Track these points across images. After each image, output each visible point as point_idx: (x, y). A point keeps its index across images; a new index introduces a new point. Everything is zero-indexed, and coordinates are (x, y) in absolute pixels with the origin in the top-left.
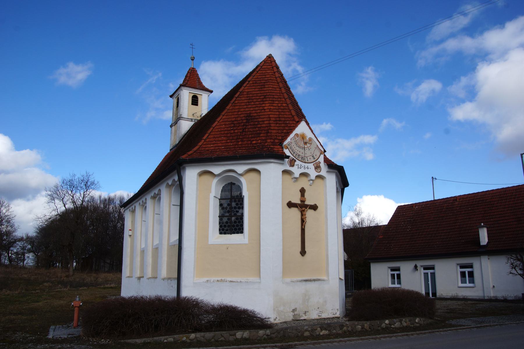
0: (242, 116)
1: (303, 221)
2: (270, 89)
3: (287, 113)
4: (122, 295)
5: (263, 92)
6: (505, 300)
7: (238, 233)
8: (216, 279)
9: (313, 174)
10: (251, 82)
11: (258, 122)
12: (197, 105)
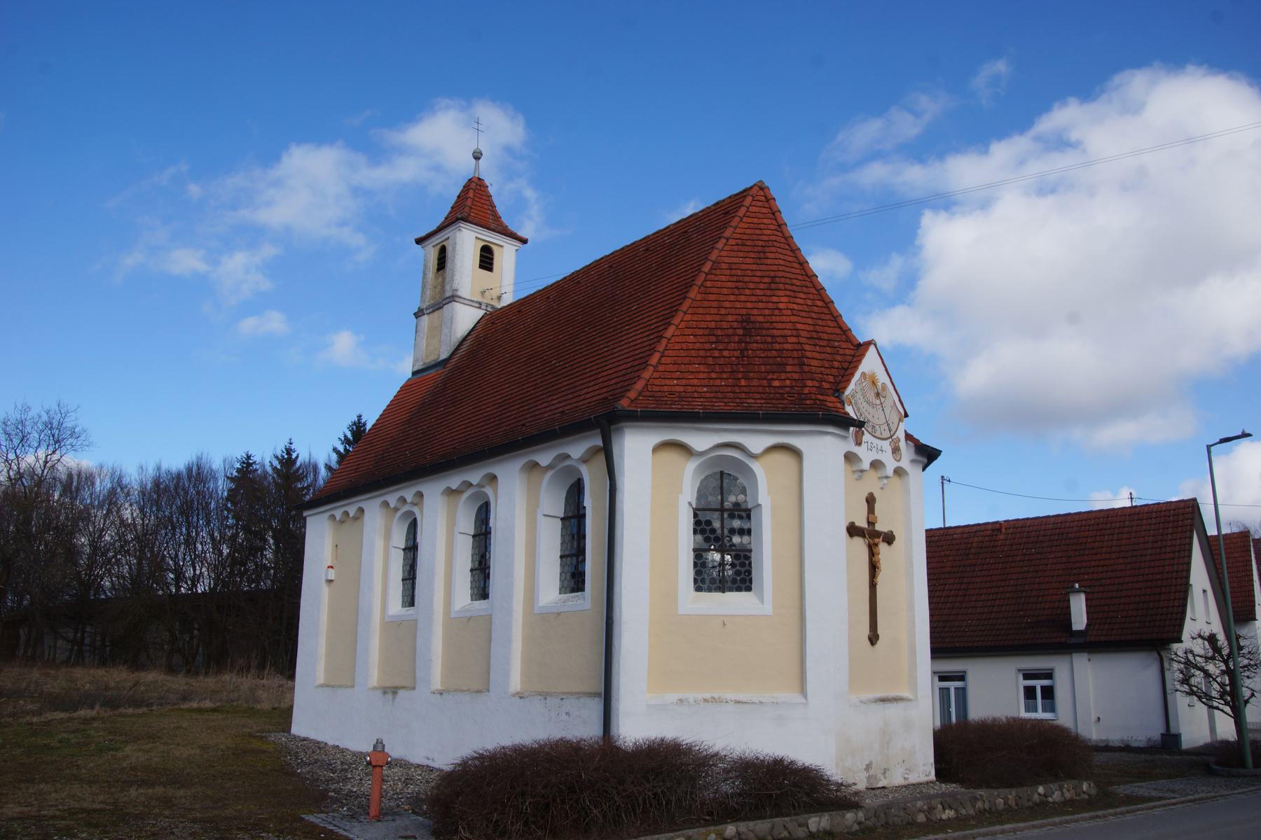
0: (730, 318)
1: (874, 568)
2: (781, 262)
3: (830, 323)
4: (301, 726)
5: (764, 267)
6: (1127, 748)
7: (739, 589)
8: (700, 696)
9: (890, 464)
10: (732, 242)
11: (773, 337)
12: (490, 270)
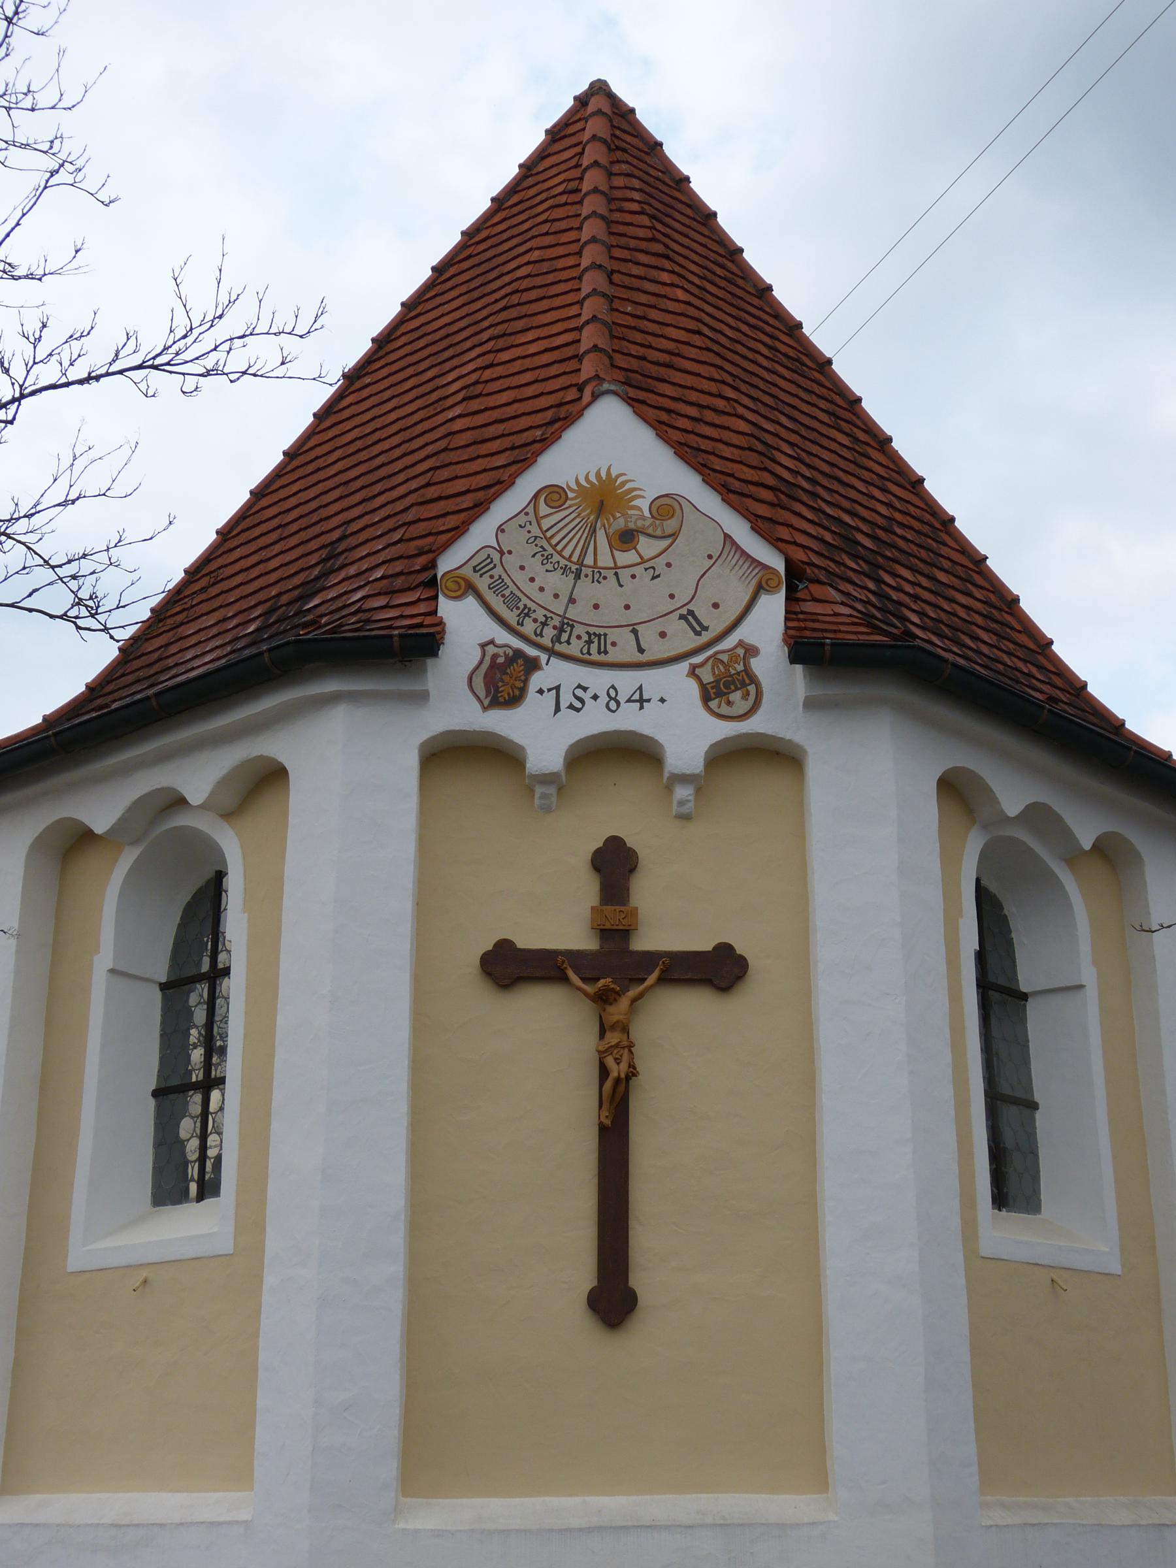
9: (686, 730)
